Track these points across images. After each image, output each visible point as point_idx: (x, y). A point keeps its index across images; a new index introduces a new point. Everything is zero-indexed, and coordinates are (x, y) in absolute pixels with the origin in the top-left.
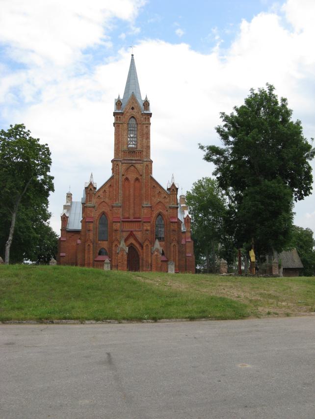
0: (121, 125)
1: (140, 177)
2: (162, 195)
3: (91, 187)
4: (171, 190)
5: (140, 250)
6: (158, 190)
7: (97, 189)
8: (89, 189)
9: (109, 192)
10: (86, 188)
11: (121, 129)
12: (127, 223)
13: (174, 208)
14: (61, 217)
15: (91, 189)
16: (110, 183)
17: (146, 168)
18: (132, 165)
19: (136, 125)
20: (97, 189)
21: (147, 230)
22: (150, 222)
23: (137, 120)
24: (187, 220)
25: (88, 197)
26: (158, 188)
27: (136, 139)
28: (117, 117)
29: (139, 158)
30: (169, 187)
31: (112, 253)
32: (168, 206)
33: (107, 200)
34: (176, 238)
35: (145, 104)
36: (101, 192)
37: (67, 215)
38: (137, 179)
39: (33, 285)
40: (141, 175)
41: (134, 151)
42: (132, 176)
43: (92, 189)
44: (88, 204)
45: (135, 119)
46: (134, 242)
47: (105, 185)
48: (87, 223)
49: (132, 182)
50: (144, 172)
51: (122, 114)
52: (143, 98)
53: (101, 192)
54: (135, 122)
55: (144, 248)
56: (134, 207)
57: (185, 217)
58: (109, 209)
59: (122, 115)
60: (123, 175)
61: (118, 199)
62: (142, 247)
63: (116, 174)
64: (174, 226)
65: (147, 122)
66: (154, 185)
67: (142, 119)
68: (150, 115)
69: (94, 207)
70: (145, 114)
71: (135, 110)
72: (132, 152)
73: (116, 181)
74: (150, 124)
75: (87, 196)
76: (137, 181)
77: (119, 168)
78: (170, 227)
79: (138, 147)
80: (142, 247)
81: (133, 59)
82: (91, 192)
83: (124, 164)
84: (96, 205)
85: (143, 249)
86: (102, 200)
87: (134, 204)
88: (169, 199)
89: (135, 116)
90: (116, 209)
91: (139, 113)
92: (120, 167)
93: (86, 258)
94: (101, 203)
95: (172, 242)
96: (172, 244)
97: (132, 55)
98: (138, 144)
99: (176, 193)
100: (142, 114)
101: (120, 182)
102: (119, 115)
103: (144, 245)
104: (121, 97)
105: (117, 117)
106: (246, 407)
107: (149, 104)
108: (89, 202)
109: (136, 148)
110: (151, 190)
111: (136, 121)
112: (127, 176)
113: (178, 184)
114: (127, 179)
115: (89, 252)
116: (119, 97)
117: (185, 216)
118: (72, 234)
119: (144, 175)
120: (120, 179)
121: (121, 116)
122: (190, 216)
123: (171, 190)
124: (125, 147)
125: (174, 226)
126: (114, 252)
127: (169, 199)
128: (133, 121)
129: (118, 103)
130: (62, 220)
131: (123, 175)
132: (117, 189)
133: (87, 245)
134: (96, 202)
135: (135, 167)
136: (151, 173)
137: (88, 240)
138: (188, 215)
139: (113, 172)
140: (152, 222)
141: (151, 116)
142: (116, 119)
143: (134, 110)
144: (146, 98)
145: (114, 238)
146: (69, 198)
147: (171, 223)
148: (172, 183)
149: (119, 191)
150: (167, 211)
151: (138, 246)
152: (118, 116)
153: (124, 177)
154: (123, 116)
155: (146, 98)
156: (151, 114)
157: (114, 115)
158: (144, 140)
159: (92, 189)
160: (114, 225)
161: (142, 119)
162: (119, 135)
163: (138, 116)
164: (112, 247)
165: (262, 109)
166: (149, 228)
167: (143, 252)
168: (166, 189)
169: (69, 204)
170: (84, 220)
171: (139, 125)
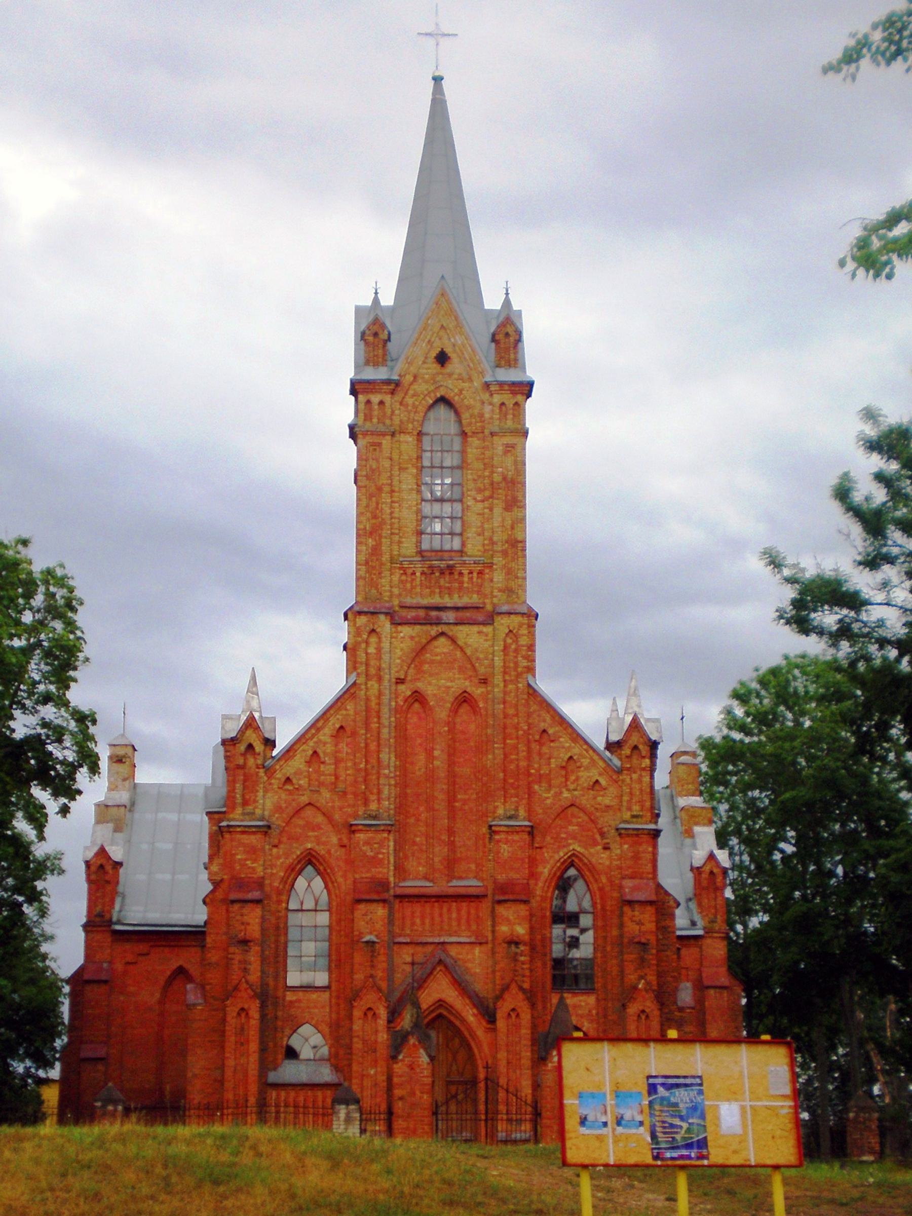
0: (386, 441)
1: (478, 691)
2: (583, 774)
3: (251, 736)
4: (627, 751)
5: (480, 1033)
6: (564, 748)
7: (282, 744)
8: (242, 747)
9: (337, 762)
10: (228, 743)
11: (387, 464)
12: (417, 908)
13: (638, 833)
14: (88, 864)
15: (250, 747)
16: (343, 720)
17: (506, 648)
18: (443, 634)
19: (457, 441)
20: (282, 744)
21: (513, 942)
22: (525, 902)
23: (465, 416)
24: (707, 879)
25: (239, 786)
26: (565, 741)
27: (458, 507)
28: (368, 402)
29: (475, 599)
30: (614, 738)
31: (350, 1047)
32: (609, 821)
33: (325, 797)
34: (652, 978)
35: (500, 337)
36: (298, 763)
37: (116, 853)
38: (464, 699)
39: (271, 1154)
40: (484, 682)
41: (451, 568)
42: (440, 686)
43: (259, 747)
44: (237, 818)
45: (457, 413)
46: (451, 995)
47: (315, 726)
48: (236, 906)
49: (442, 714)
50: (498, 662)
51: (394, 386)
52: (492, 301)
53: (298, 763)
54: (453, 428)
55: (501, 1024)
56: (451, 831)
57: (697, 863)
58: (334, 840)
59: (393, 393)
60: (400, 681)
61: (379, 792)
62: (490, 1016)
63: (368, 677)
64: (640, 923)
65: (509, 424)
66: (543, 725)
67: (487, 409)
68: (527, 388)
69: (266, 830)
70: (501, 384)
71: (455, 366)
72: (442, 568)
73: (368, 709)
74: (525, 434)
75: (231, 783)
76: (465, 708)
77: (379, 649)
78: (621, 926)
79: (469, 549)
80: (490, 1016)
81: (444, 102)
82: (251, 762)
83: (406, 631)
84: (277, 821)
85: (494, 1030)
86: (304, 799)
87: (452, 813)
88: (613, 790)
89: (450, 395)
90: (367, 843)
91: (470, 380)
92: (386, 645)
93: (229, 1073)
94: (298, 812)
95: (632, 999)
96: (633, 1009)
97: (438, 80)
98: (471, 534)
99: (647, 762)
100: (487, 385)
101: (385, 711)
102: (372, 391)
103: (500, 1015)
104: (388, 299)
105: (368, 402)
106: (588, 1069)
107: (519, 334)
108: (239, 810)
109: (461, 552)
110: (529, 751)
111: (459, 421)
112: (420, 685)
113: (657, 721)
114: (418, 697)
115: (242, 1042)
116: (376, 301)
117: (699, 857)
118: (143, 947)
119: (498, 680)
120: (385, 699)
121: (387, 399)
122: (722, 856)
123: (627, 751)
124: (408, 547)
125: (640, 923)
126: (358, 1045)
127: (613, 790)
128: (441, 423)
129: (374, 336)
130: (89, 880)
131: (400, 681)
132: (373, 746)
133: (232, 1012)
134: (278, 809)
135: (453, 640)
136: (531, 670)
137: (236, 988)
138: (711, 857)
139: (352, 665)
140: (534, 903)
141: (529, 395)
142: (364, 411)
143: (449, 368)
144: (507, 303)
145: (359, 977)
146: (123, 769)
147: (626, 909)
148: (629, 719)
149: (384, 756)
150: (606, 848)
151: (470, 1015)
152: (375, 399)
153: (405, 690)
154: (398, 397)
155: (507, 303)
156: (531, 385)
157: (354, 392)
158: (497, 511)
159: (259, 747)
160: (358, 914)
161: (487, 409)
162: (380, 489)
163: (470, 397)
164: (350, 1018)
165: (773, 831)
166: (521, 930)
167: (494, 1046)
168: (600, 744)
169: (123, 796)
170: (220, 895)
171: (474, 441)
